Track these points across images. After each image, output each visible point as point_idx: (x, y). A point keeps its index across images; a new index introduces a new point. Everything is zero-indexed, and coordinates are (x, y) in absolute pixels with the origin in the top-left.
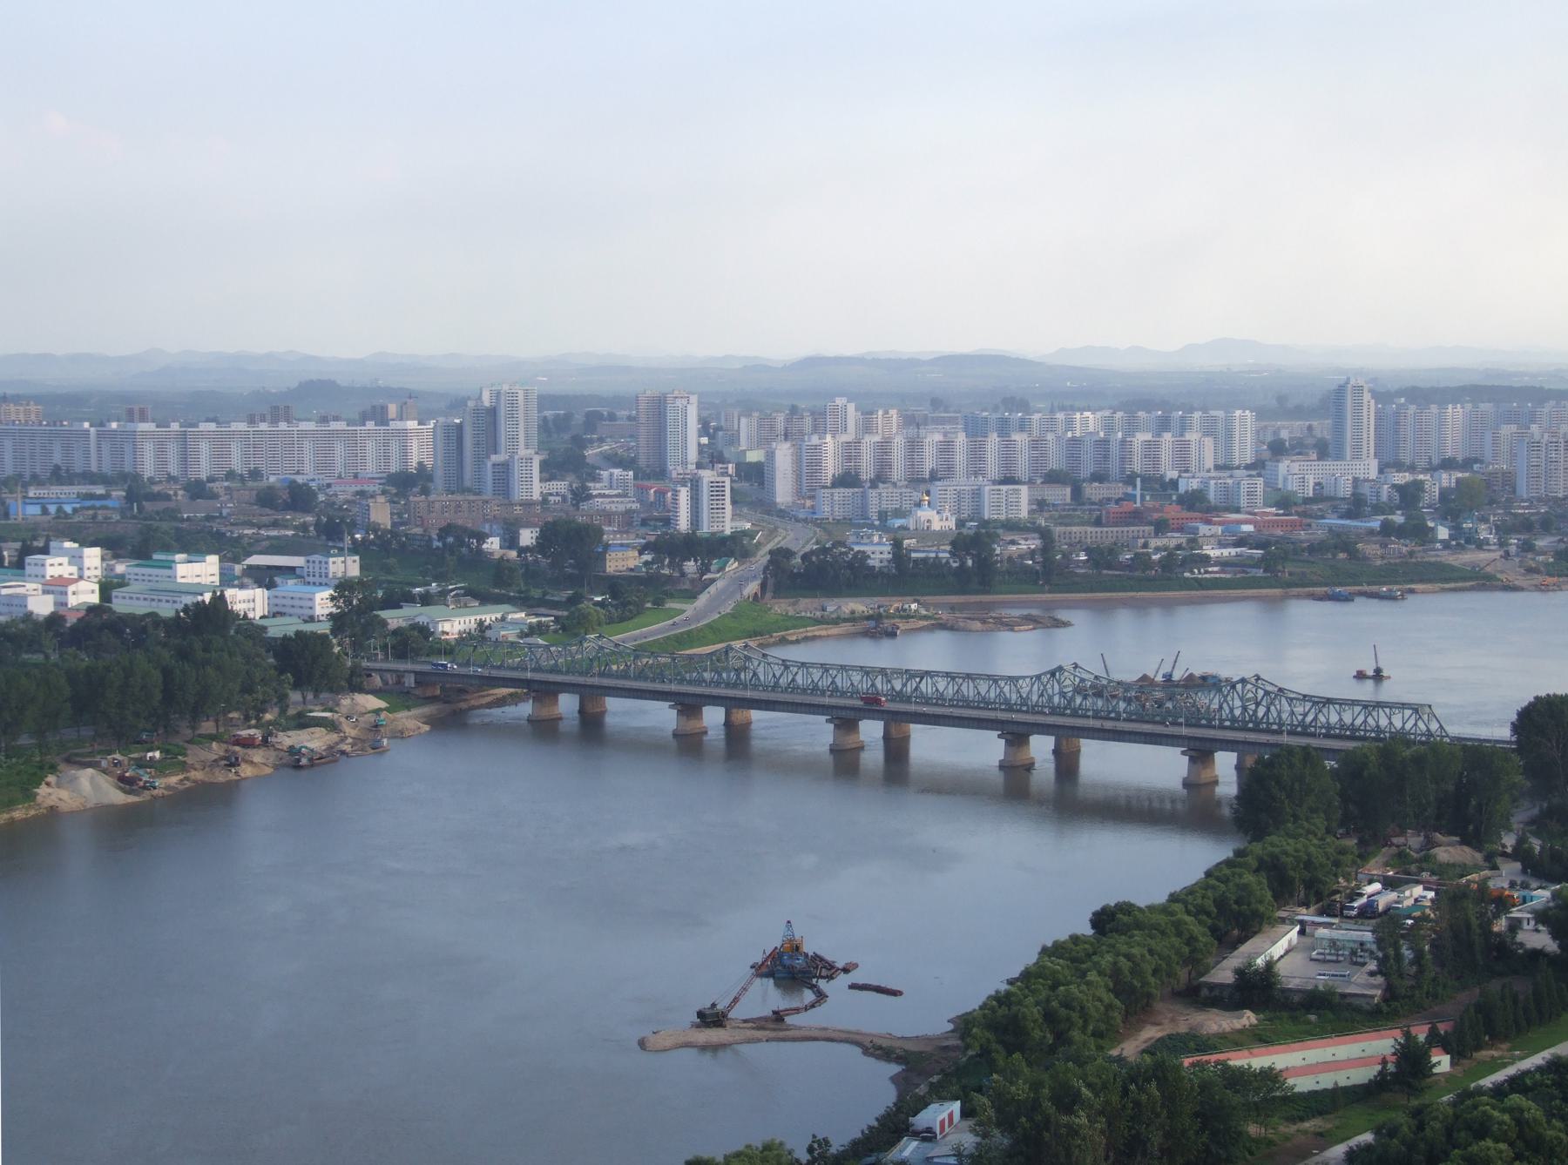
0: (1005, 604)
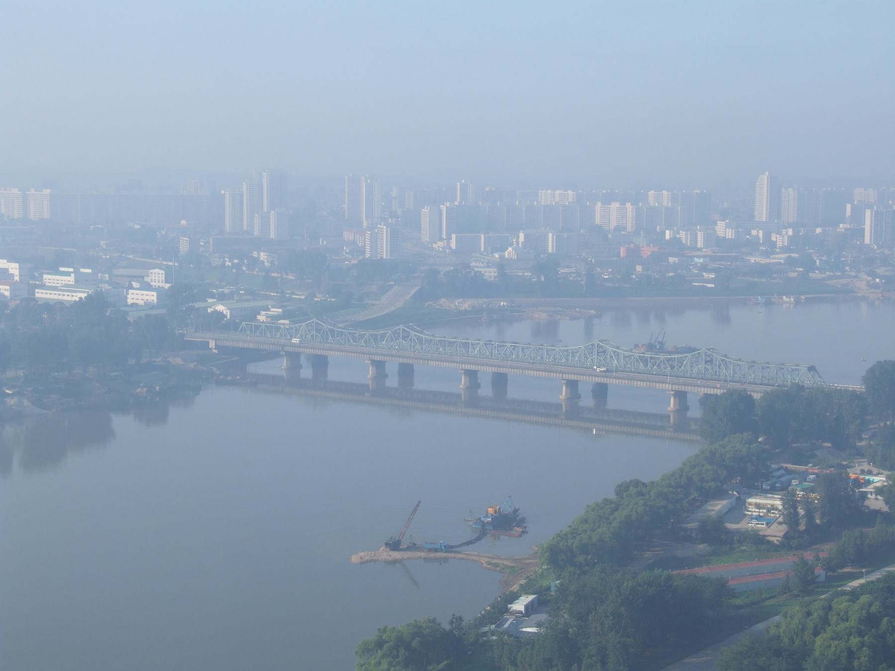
0: (67, 288)
